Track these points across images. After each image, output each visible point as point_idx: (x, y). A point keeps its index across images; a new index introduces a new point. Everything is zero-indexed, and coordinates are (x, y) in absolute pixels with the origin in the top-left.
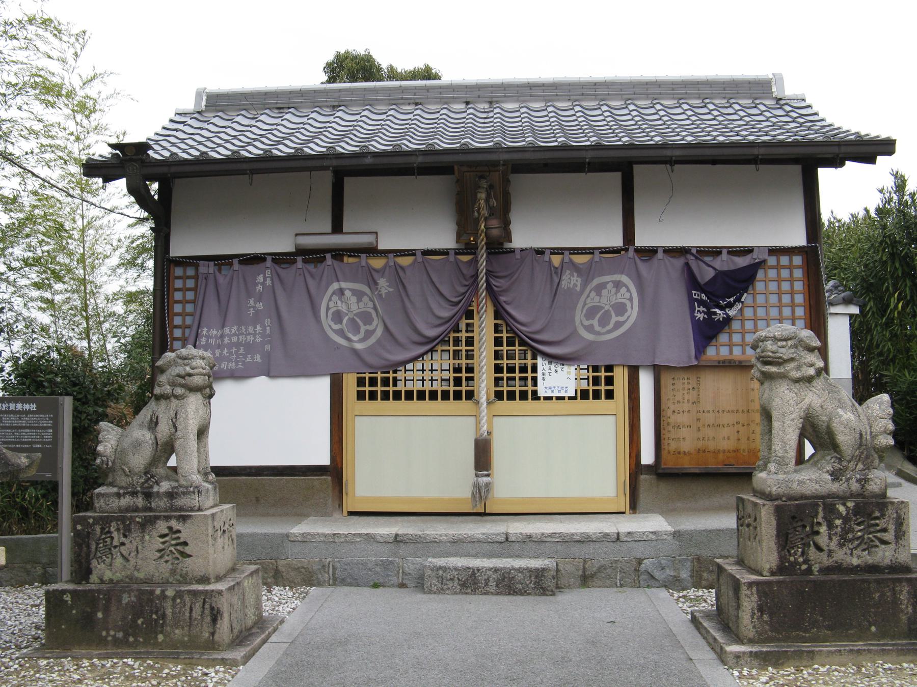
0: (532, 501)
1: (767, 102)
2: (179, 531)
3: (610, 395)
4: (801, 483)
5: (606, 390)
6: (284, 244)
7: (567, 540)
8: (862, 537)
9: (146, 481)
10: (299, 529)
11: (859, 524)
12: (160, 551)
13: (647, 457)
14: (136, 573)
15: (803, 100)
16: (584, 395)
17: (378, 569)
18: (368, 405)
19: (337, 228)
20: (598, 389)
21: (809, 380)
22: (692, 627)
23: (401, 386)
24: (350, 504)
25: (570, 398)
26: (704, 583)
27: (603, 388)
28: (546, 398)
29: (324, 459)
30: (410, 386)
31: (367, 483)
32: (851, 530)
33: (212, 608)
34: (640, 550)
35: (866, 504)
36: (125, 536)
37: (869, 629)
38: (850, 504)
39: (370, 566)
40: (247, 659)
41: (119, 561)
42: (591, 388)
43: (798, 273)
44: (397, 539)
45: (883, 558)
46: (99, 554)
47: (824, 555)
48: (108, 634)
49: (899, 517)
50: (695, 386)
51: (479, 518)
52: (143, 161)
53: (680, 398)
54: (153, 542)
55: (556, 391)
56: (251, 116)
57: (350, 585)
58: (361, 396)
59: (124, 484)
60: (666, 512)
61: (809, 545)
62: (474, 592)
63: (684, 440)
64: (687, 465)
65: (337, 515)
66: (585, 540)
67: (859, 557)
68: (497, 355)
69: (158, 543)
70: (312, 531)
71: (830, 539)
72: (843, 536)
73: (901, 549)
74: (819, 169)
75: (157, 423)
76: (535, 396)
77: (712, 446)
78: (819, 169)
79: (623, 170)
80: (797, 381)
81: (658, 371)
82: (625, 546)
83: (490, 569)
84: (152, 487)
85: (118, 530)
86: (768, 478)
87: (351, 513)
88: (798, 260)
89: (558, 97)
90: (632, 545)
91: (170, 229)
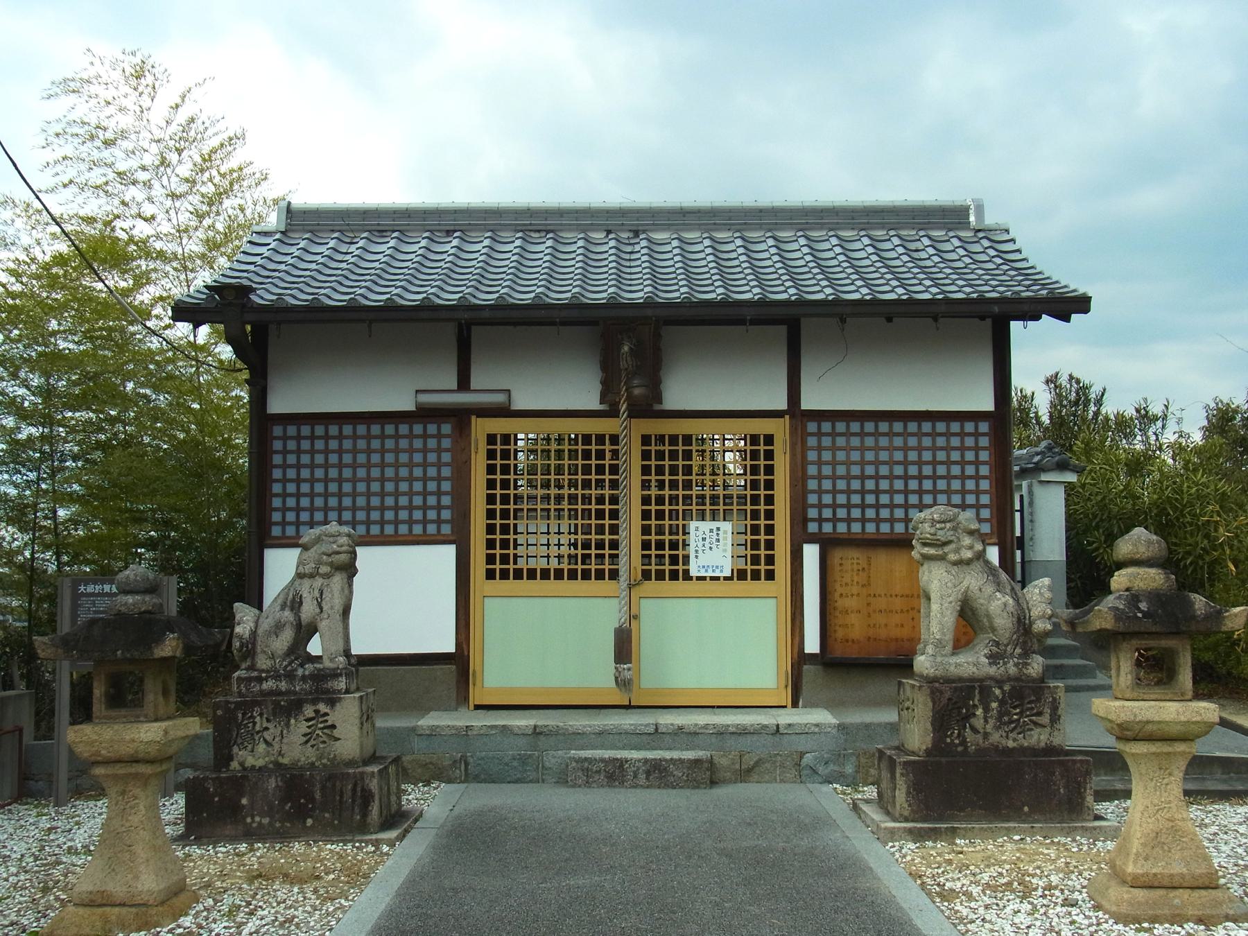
0: (684, 691)
1: (962, 234)
2: (326, 714)
3: (770, 576)
4: (957, 665)
5: (766, 540)
6: (404, 402)
7: (722, 733)
8: (1018, 720)
9: (290, 664)
10: (429, 721)
11: (1015, 708)
12: (305, 735)
13: (812, 645)
14: (281, 760)
15: (1007, 231)
16: (742, 575)
17: (515, 764)
18: (498, 585)
19: (464, 384)
20: (755, 566)
21: (968, 562)
22: (853, 814)
23: (522, 564)
24: (476, 697)
25: (726, 578)
26: (871, 779)
27: (763, 567)
28: (699, 578)
29: (450, 648)
30: (532, 564)
31: (497, 673)
32: (1008, 714)
33: (363, 790)
34: (802, 744)
35: (1021, 687)
36: (268, 720)
37: (1021, 809)
38: (1007, 688)
39: (506, 760)
40: (401, 838)
41: (262, 747)
42: (749, 567)
43: (984, 442)
44: (536, 732)
45: (1039, 741)
46: (239, 741)
47: (979, 738)
48: (253, 821)
49: (1055, 699)
50: (866, 566)
51: (623, 711)
52: (244, 306)
53: (849, 581)
54: (300, 727)
55: (710, 570)
56: (348, 240)
57: (485, 781)
58: (490, 575)
59: (264, 667)
60: (830, 705)
61: (965, 727)
62: (622, 783)
63: (854, 627)
64: (852, 653)
65: (463, 710)
66: (742, 732)
67: (1015, 740)
68: (646, 530)
69: (303, 727)
70: (436, 723)
71: (986, 721)
72: (999, 718)
73: (1056, 733)
74: (1012, 323)
75: (301, 603)
76: (687, 576)
77: (883, 633)
78: (1012, 323)
79: (790, 328)
80: (955, 563)
81: (828, 545)
82: (786, 738)
83: (639, 761)
84: (296, 670)
85: (261, 715)
86: (922, 663)
87: (478, 707)
88: (984, 427)
89: (717, 227)
90: (793, 737)
91: (266, 379)
